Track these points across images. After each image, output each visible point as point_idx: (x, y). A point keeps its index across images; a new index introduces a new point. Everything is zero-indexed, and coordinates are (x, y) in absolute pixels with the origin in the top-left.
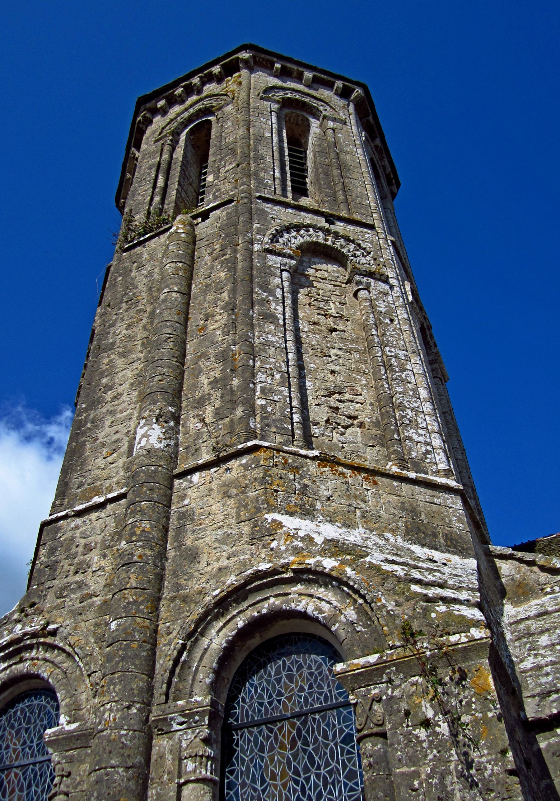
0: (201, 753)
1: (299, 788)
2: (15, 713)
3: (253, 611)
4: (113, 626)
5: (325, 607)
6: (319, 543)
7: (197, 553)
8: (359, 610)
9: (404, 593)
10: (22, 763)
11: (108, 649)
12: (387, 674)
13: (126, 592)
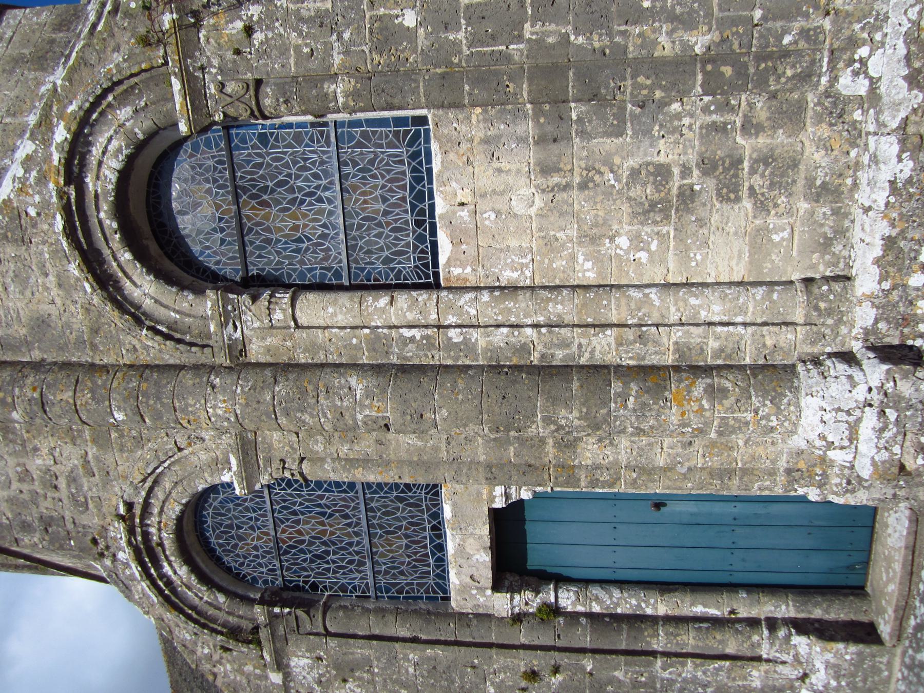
0: (267, 303)
1: (308, 199)
2: (220, 545)
3: (114, 239)
4: (119, 416)
5: (115, 144)
6: (34, 147)
7: (38, 319)
8: (122, 100)
9: (104, 39)
10: (272, 526)
11: (147, 421)
12: (195, 71)
13: (78, 403)
